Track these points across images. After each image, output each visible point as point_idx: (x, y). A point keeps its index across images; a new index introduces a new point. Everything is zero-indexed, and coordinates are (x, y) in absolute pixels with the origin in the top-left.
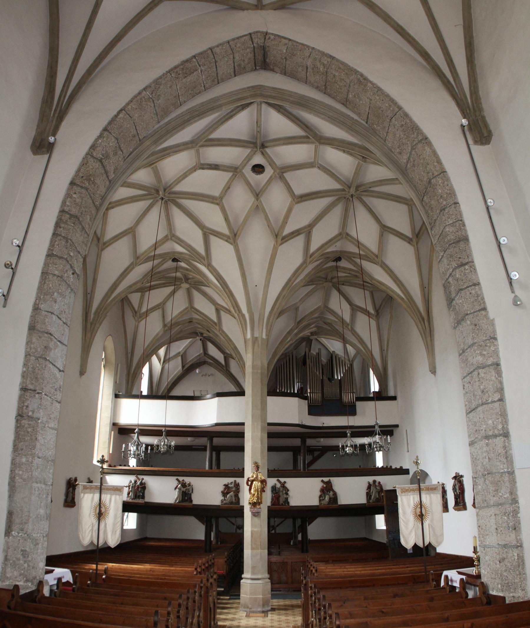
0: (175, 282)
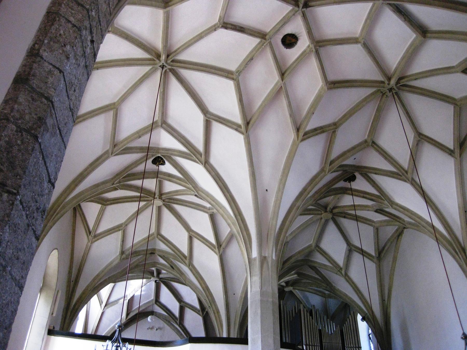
0: (145, 195)
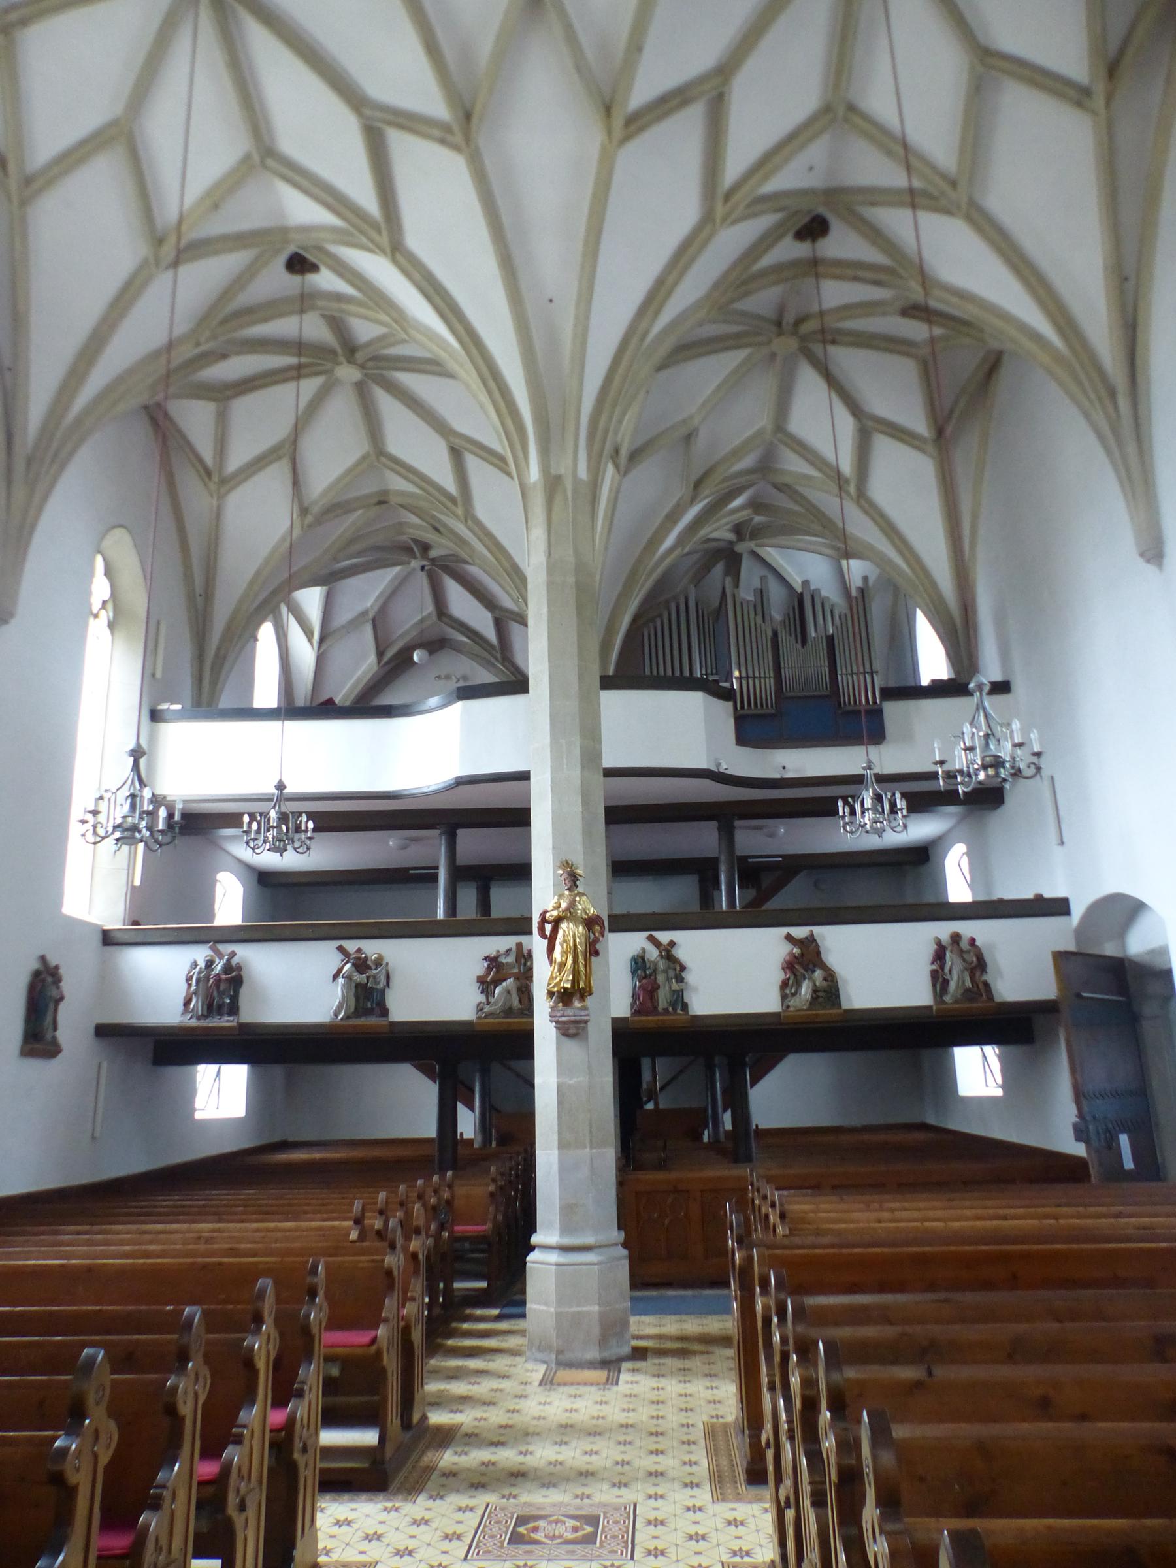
0: (308, 359)
